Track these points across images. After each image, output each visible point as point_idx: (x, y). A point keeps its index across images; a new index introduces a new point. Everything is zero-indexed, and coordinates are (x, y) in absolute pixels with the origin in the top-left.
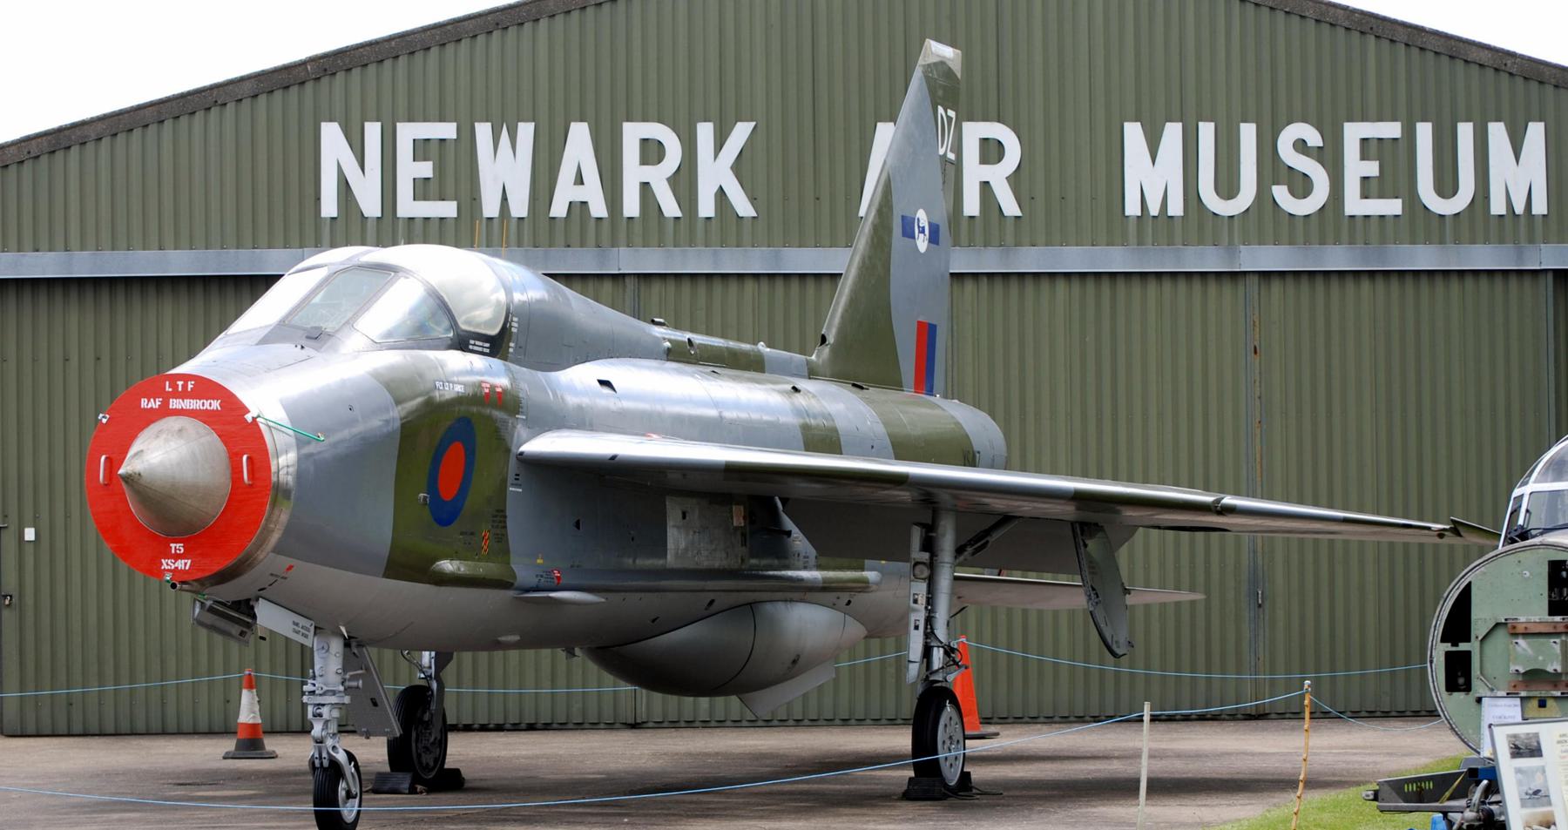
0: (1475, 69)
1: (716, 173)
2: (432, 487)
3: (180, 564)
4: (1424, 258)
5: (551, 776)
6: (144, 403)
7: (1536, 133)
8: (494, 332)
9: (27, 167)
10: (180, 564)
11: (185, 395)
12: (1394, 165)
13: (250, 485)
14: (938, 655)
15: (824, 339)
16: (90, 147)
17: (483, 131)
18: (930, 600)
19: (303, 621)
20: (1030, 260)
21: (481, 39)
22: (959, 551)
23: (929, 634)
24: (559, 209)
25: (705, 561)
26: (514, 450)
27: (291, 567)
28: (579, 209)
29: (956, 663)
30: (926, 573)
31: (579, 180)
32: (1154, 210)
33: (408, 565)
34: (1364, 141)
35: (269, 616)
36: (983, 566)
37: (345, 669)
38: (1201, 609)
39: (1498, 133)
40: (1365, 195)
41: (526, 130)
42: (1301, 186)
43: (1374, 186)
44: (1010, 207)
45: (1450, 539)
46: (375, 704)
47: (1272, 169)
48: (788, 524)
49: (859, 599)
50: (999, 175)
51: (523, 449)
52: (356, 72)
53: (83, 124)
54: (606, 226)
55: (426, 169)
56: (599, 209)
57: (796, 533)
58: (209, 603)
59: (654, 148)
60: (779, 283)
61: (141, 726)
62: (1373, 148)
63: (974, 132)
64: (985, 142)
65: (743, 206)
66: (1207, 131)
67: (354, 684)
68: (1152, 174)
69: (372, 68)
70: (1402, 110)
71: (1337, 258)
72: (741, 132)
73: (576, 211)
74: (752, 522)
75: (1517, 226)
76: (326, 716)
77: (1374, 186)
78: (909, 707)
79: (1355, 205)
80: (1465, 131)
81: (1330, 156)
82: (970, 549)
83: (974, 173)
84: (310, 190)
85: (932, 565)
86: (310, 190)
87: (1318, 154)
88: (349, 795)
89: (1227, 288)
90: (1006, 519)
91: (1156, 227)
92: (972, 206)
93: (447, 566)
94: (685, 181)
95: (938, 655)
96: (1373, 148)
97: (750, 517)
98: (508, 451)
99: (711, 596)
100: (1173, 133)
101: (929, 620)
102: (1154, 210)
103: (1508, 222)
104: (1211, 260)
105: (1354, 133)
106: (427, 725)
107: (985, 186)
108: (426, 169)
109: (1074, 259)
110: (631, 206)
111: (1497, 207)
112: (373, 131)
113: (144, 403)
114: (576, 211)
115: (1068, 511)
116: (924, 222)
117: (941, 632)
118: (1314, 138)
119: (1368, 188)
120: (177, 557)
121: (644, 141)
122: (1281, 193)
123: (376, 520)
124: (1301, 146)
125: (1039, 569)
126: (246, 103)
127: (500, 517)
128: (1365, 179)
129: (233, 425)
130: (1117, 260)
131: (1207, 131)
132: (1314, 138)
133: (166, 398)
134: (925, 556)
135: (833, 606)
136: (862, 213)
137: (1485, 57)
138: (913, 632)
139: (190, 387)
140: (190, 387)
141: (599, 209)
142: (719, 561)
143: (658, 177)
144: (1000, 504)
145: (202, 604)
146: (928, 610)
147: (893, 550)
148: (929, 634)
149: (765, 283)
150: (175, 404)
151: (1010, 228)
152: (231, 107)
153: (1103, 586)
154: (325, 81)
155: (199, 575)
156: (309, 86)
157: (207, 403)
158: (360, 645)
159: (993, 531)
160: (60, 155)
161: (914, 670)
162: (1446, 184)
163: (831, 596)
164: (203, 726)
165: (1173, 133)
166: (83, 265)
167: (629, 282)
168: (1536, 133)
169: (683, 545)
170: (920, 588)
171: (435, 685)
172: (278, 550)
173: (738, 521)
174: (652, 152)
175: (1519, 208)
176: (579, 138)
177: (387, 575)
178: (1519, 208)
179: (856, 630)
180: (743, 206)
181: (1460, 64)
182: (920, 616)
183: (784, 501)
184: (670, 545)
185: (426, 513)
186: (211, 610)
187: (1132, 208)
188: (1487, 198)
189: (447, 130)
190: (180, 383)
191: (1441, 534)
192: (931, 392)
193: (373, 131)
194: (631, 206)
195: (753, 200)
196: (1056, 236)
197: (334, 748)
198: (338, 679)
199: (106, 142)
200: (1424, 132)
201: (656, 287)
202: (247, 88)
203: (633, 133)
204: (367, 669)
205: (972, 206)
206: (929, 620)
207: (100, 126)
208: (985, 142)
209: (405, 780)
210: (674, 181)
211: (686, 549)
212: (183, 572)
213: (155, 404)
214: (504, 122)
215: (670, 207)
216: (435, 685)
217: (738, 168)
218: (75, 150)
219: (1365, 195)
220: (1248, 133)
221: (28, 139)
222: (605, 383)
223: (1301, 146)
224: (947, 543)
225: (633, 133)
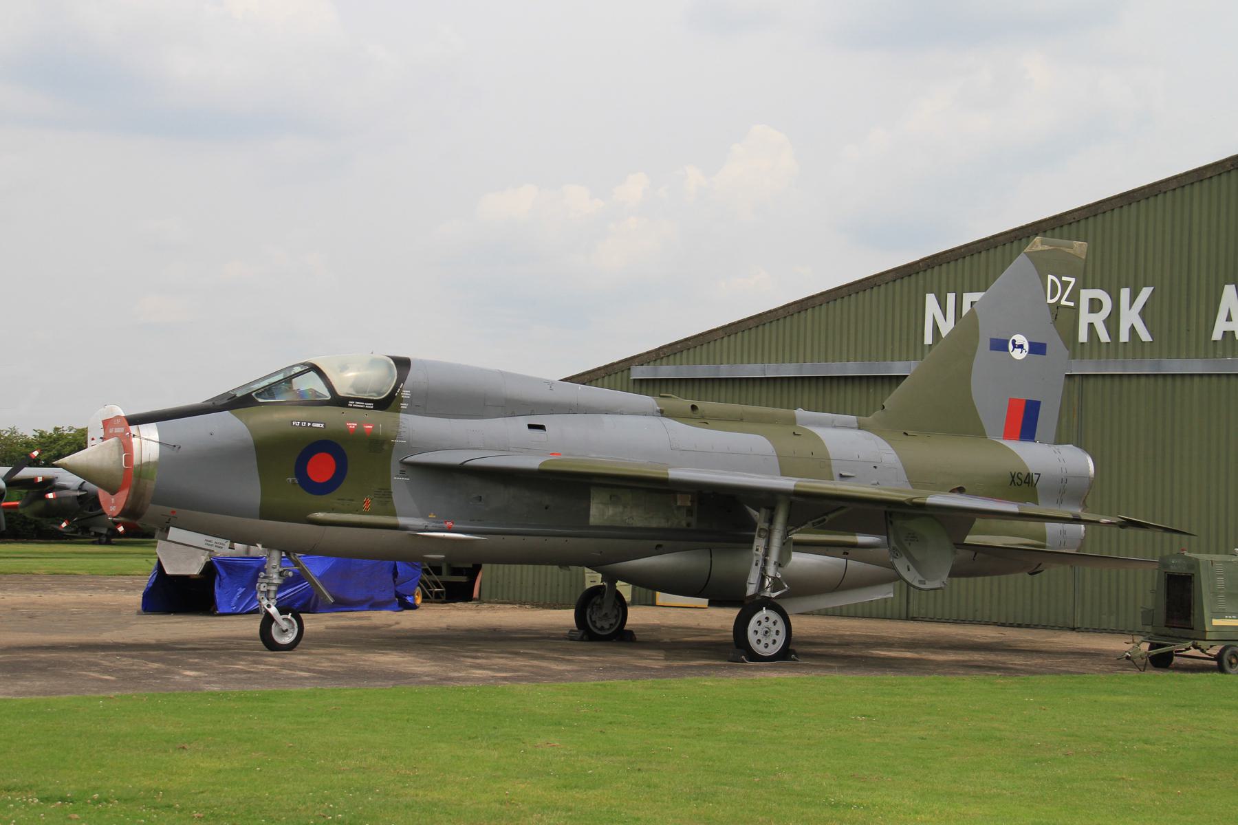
1: (1130, 317)
5: (523, 631)
9: (788, 319)
21: (1008, 245)
23: (764, 570)
24: (1217, 335)
52: (944, 266)
53: (813, 297)
59: (1097, 303)
60: (1160, 381)
61: (889, 614)
63: (1086, 295)
64: (1092, 300)
65: (1145, 336)
69: (952, 264)
72: (1146, 293)
78: (574, 601)
83: (1085, 317)
84: (919, 330)
86: (919, 330)
92: (1083, 337)
93: (319, 515)
94: (1112, 322)
101: (765, 561)
107: (1091, 325)
112: (951, 298)
143: (1098, 319)
148: (764, 570)
149: (1152, 380)
152: (883, 286)
154: (929, 271)
156: (921, 274)
164: (889, 614)
166: (808, 370)
167: (1077, 379)
174: (1095, 305)
177: (261, 518)
180: (1145, 336)
193: (951, 298)
196: (1175, 352)
199: (824, 306)
201: (1092, 381)
205: (1083, 337)
208: (1092, 300)
210: (1107, 322)
217: (1143, 314)
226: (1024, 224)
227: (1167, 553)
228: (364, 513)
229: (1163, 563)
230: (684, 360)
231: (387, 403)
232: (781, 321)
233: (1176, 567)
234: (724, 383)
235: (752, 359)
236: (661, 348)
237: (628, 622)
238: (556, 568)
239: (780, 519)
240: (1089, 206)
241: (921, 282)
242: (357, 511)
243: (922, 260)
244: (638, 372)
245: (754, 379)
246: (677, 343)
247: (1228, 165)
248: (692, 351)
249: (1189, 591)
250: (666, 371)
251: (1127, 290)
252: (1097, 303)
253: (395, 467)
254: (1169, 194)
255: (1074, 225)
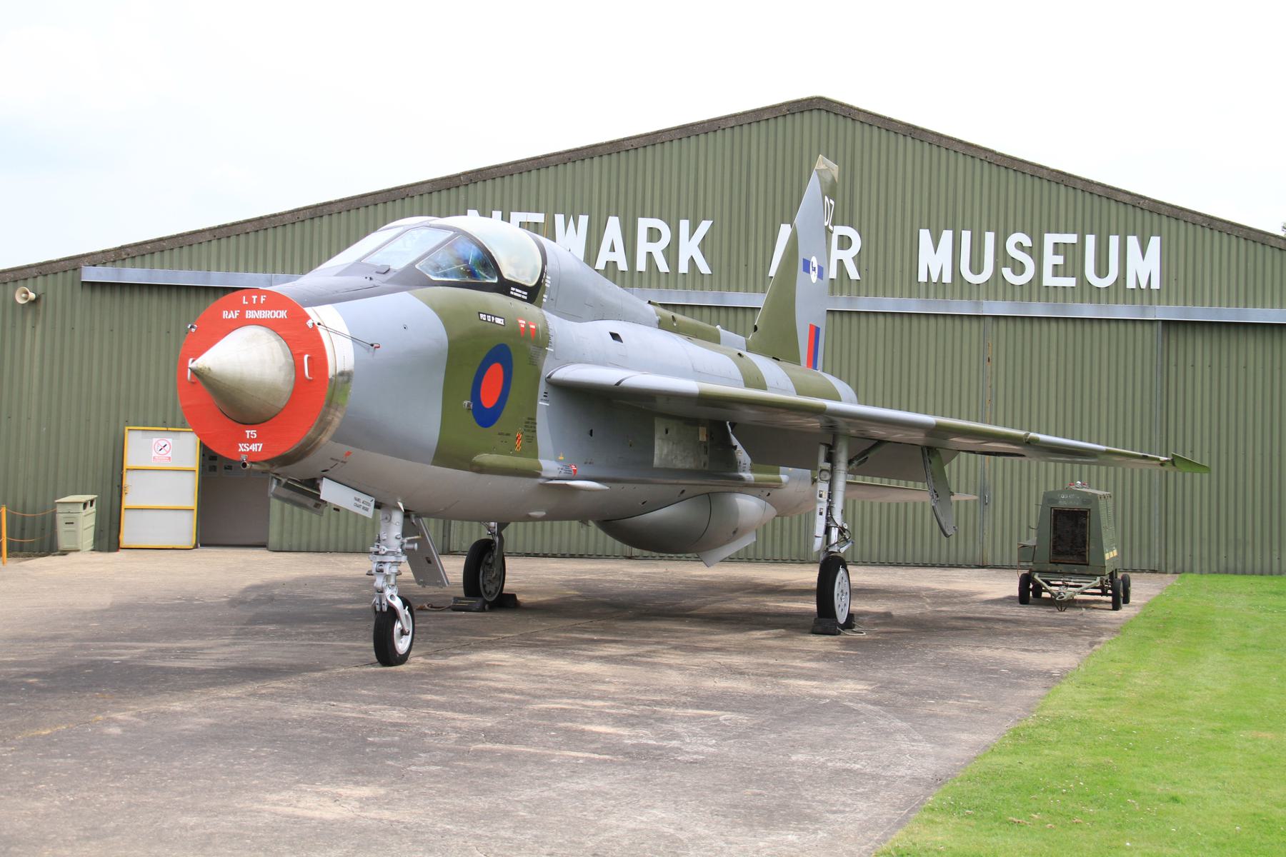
0: (1121, 205)
1: (690, 249)
2: (475, 396)
3: (254, 447)
4: (1088, 311)
6: (225, 315)
7: (1155, 242)
8: (532, 284)
9: (298, 226)
10: (254, 447)
11: (258, 307)
12: (1072, 260)
13: (313, 381)
14: (834, 533)
15: (756, 328)
16: (335, 217)
17: (559, 219)
18: (830, 496)
19: (364, 498)
20: (864, 304)
22: (850, 462)
23: (829, 518)
25: (679, 464)
26: (545, 373)
27: (349, 453)
28: (611, 265)
29: (846, 539)
30: (828, 477)
31: (613, 249)
32: (935, 279)
33: (447, 456)
34: (1056, 244)
35: (330, 491)
36: (864, 474)
37: (404, 535)
38: (971, 505)
39: (1133, 241)
40: (1055, 274)
41: (584, 220)
42: (1019, 268)
43: (1061, 270)
44: (854, 274)
45: (1168, 467)
46: (429, 562)
47: (1002, 257)
48: (735, 442)
49: (775, 493)
50: (848, 256)
51: (554, 376)
53: (330, 203)
54: (627, 276)
55: (1059, 260)
56: (622, 266)
57: (740, 448)
58: (284, 481)
61: (323, 547)
62: (1061, 248)
65: (704, 268)
66: (966, 235)
67: (410, 546)
68: (934, 259)
69: (498, 181)
70: (1079, 228)
71: (1038, 310)
72: (705, 226)
73: (611, 266)
74: (712, 439)
75: (1143, 294)
76: (387, 571)
77: (1061, 270)
79: (1049, 280)
80: (1114, 241)
81: (1036, 252)
82: (856, 462)
85: (832, 472)
87: (1029, 251)
88: (403, 633)
89: (975, 323)
90: (880, 442)
91: (935, 288)
94: (672, 252)
95: (834, 533)
96: (1061, 248)
97: (710, 435)
98: (538, 374)
99: (684, 488)
100: (947, 235)
101: (830, 509)
102: (935, 279)
103: (1137, 293)
104: (966, 308)
105: (1050, 239)
106: (491, 565)
108: (1059, 260)
109: (888, 304)
110: (641, 265)
111: (1131, 284)
113: (225, 315)
114: (611, 266)
115: (919, 438)
116: (815, 265)
117: (838, 517)
118: (1027, 242)
119: (1056, 271)
120: (251, 441)
121: (650, 229)
122: (1007, 272)
123: (424, 419)
124: (1020, 246)
125: (890, 476)
126: (426, 197)
127: (531, 425)
128: (1055, 266)
129: (299, 336)
130: (913, 306)
131: (966, 235)
132: (1027, 242)
133: (243, 309)
134: (828, 466)
135: (759, 497)
136: (772, 273)
137: (1127, 199)
138: (818, 516)
139: (262, 299)
140: (262, 299)
141: (622, 266)
142: (689, 464)
143: (658, 249)
144: (879, 432)
145: (279, 481)
146: (828, 501)
147: (802, 459)
148: (829, 518)
150: (250, 314)
151: (854, 287)
152: (417, 198)
153: (941, 489)
155: (269, 456)
156: (462, 189)
157: (276, 314)
158: (418, 516)
159: (872, 450)
160: (317, 220)
161: (818, 544)
162: (1102, 271)
163: (758, 491)
165: (947, 235)
168: (1155, 242)
169: (665, 451)
170: (823, 487)
171: (497, 539)
172: (337, 438)
173: (703, 437)
174: (654, 235)
175: (1143, 286)
176: (614, 224)
177: (433, 464)
178: (1143, 286)
179: (772, 511)
180: (704, 268)
181: (1113, 203)
182: (823, 506)
183: (733, 425)
184: (657, 451)
185: (471, 416)
186: (287, 486)
187: (922, 278)
188: (1125, 279)
189: (1072, 238)
190: (255, 297)
191: (1162, 464)
192: (815, 367)
194: (641, 265)
195: (711, 266)
197: (392, 596)
198: (398, 543)
200: (1090, 240)
202: (426, 188)
203: (644, 224)
204: (423, 535)
206: (830, 509)
207: (340, 205)
209: (477, 602)
211: (667, 455)
212: (257, 453)
213: (233, 315)
214: (572, 214)
215: (663, 267)
216: (497, 539)
217: (703, 246)
218: (326, 218)
219: (1055, 274)
220: (990, 238)
221: (298, 210)
222: (615, 336)
223: (1020, 246)
224: (842, 458)
225: (644, 224)
226: (578, 146)
227: (1051, 488)
228: (515, 454)
229: (1049, 498)
230: (167, 264)
231: (533, 294)
232: (289, 227)
233: (1065, 502)
234: (183, 292)
235: (223, 264)
236: (122, 248)
237: (506, 585)
238: (575, 523)
239: (842, 458)
240: (647, 135)
241: (462, 197)
242: (509, 451)
243: (464, 174)
244: (92, 274)
245: (179, 287)
246: (146, 243)
247: (784, 110)
248: (167, 253)
249: (1084, 526)
250: (132, 274)
251: (687, 222)
252: (656, 233)
253: (542, 387)
254: (728, 131)
255: (632, 153)
